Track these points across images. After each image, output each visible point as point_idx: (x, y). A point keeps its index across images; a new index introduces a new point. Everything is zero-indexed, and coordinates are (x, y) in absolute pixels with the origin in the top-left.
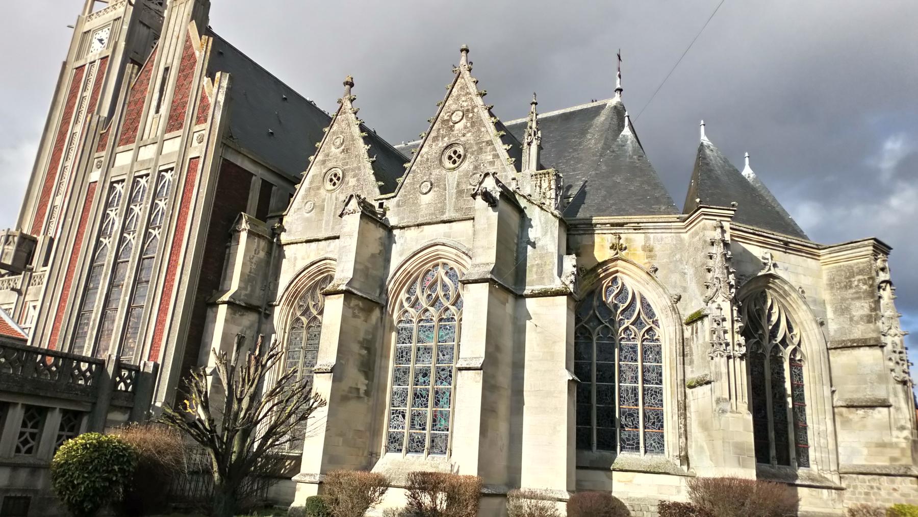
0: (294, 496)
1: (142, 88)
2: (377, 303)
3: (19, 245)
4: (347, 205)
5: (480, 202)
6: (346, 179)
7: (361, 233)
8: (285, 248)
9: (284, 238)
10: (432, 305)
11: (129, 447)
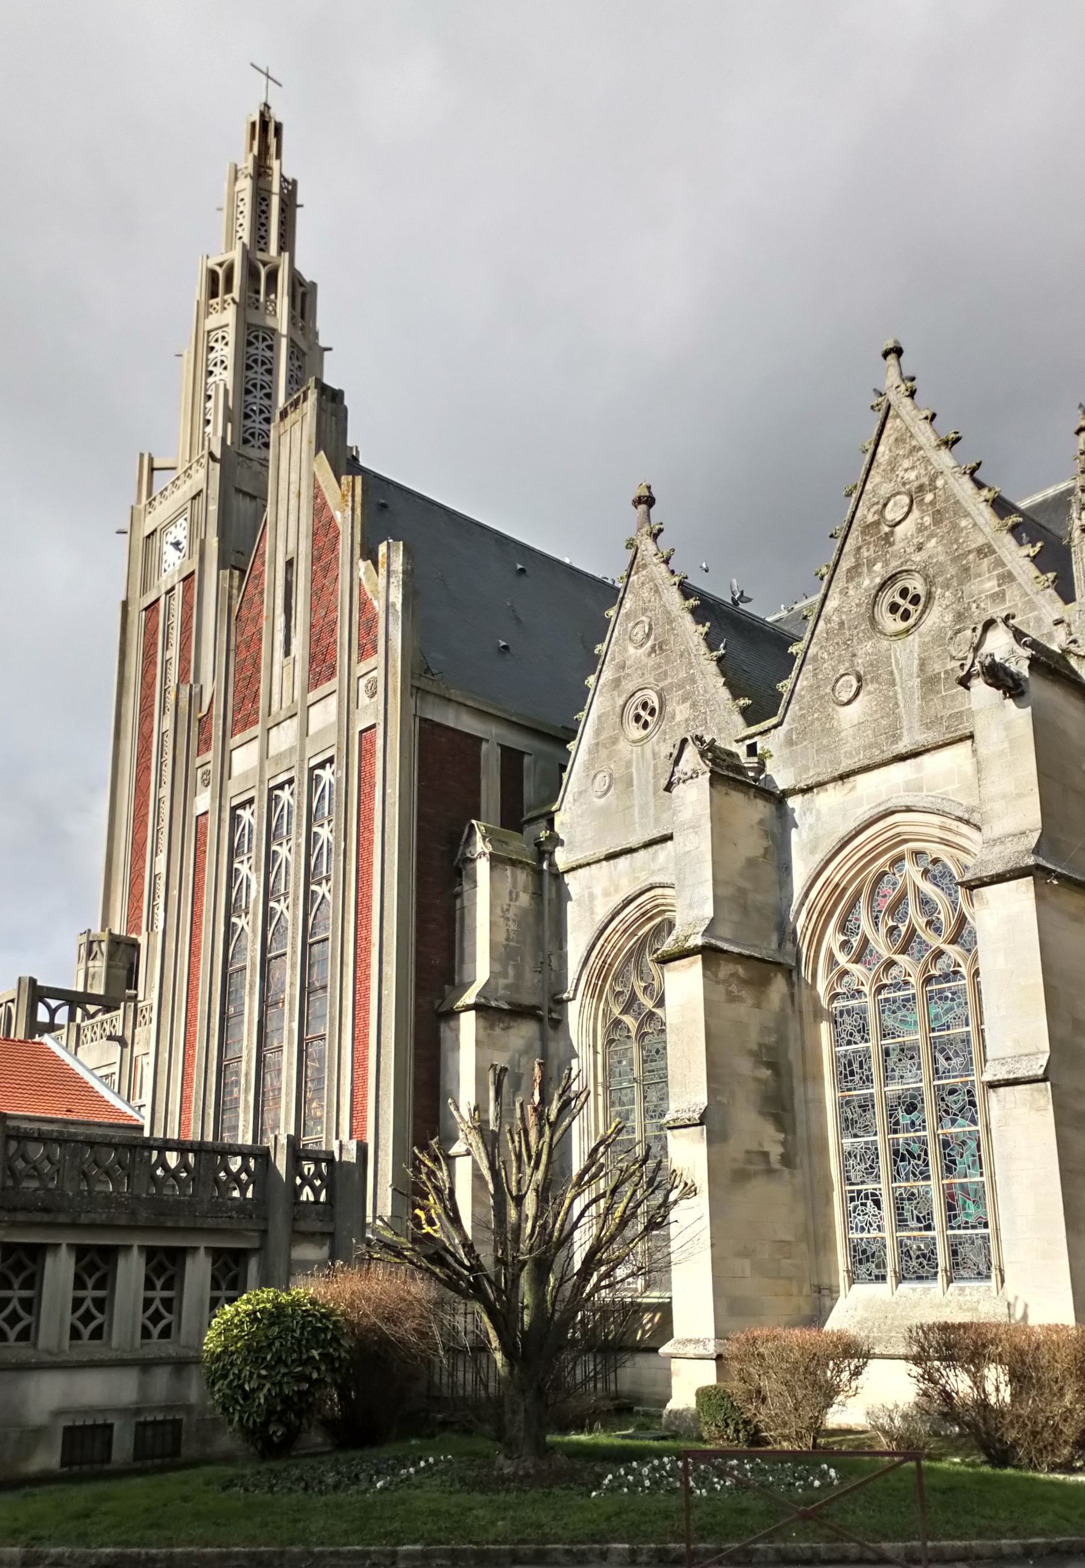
0: (669, 1386)
1: (254, 612)
2: (779, 964)
3: (111, 956)
4: (677, 762)
5: (981, 691)
6: (669, 709)
7: (719, 819)
8: (567, 878)
9: (562, 858)
10: (903, 951)
11: (332, 1312)
